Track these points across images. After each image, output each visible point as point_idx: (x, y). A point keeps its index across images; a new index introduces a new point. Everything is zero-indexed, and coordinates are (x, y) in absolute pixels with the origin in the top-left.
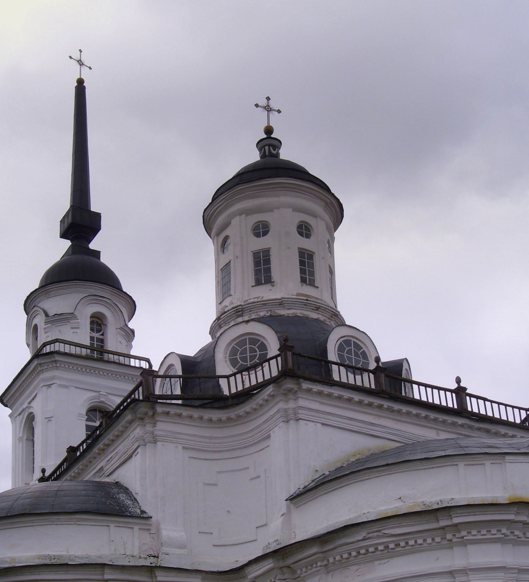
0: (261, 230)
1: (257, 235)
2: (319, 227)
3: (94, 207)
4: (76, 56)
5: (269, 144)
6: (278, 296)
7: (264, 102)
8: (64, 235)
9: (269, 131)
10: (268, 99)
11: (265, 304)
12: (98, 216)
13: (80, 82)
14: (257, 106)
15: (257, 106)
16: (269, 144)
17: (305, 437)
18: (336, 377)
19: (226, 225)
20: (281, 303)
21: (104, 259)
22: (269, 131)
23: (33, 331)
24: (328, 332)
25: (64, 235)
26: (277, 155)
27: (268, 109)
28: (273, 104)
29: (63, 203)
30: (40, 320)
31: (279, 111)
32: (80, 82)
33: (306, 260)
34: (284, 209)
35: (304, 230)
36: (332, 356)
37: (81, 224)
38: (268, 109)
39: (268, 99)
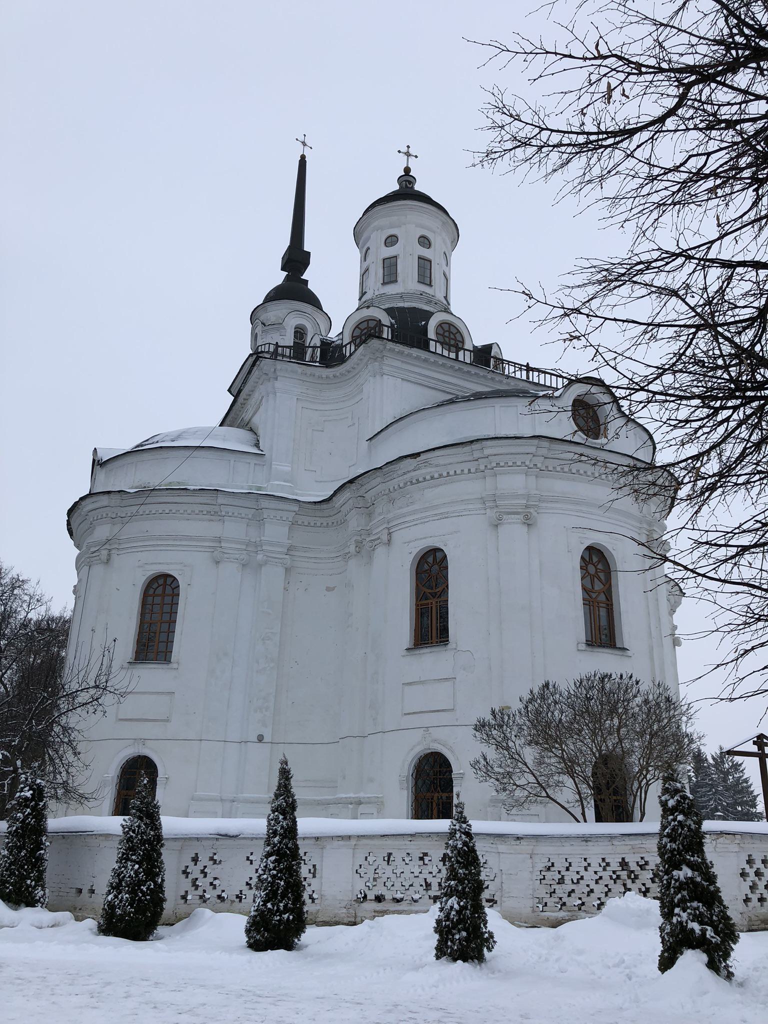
0: (391, 240)
1: (386, 244)
2: (439, 241)
3: (306, 248)
4: (301, 138)
5: (407, 178)
6: (400, 291)
7: (405, 150)
8: (282, 269)
9: (407, 170)
10: (408, 147)
11: (391, 297)
12: (309, 253)
13: (303, 158)
14: (399, 152)
15: (399, 152)
16: (407, 178)
17: (389, 386)
18: (432, 349)
19: (368, 239)
20: (401, 296)
21: (310, 286)
22: (407, 170)
23: (254, 337)
24: (428, 315)
25: (282, 269)
26: (412, 187)
27: (408, 154)
28: (411, 151)
29: (286, 242)
30: (259, 330)
31: (416, 157)
32: (303, 158)
33: (425, 265)
34: (410, 221)
35: (425, 241)
36: (431, 334)
37: (296, 259)
38: (408, 154)
39: (408, 147)
